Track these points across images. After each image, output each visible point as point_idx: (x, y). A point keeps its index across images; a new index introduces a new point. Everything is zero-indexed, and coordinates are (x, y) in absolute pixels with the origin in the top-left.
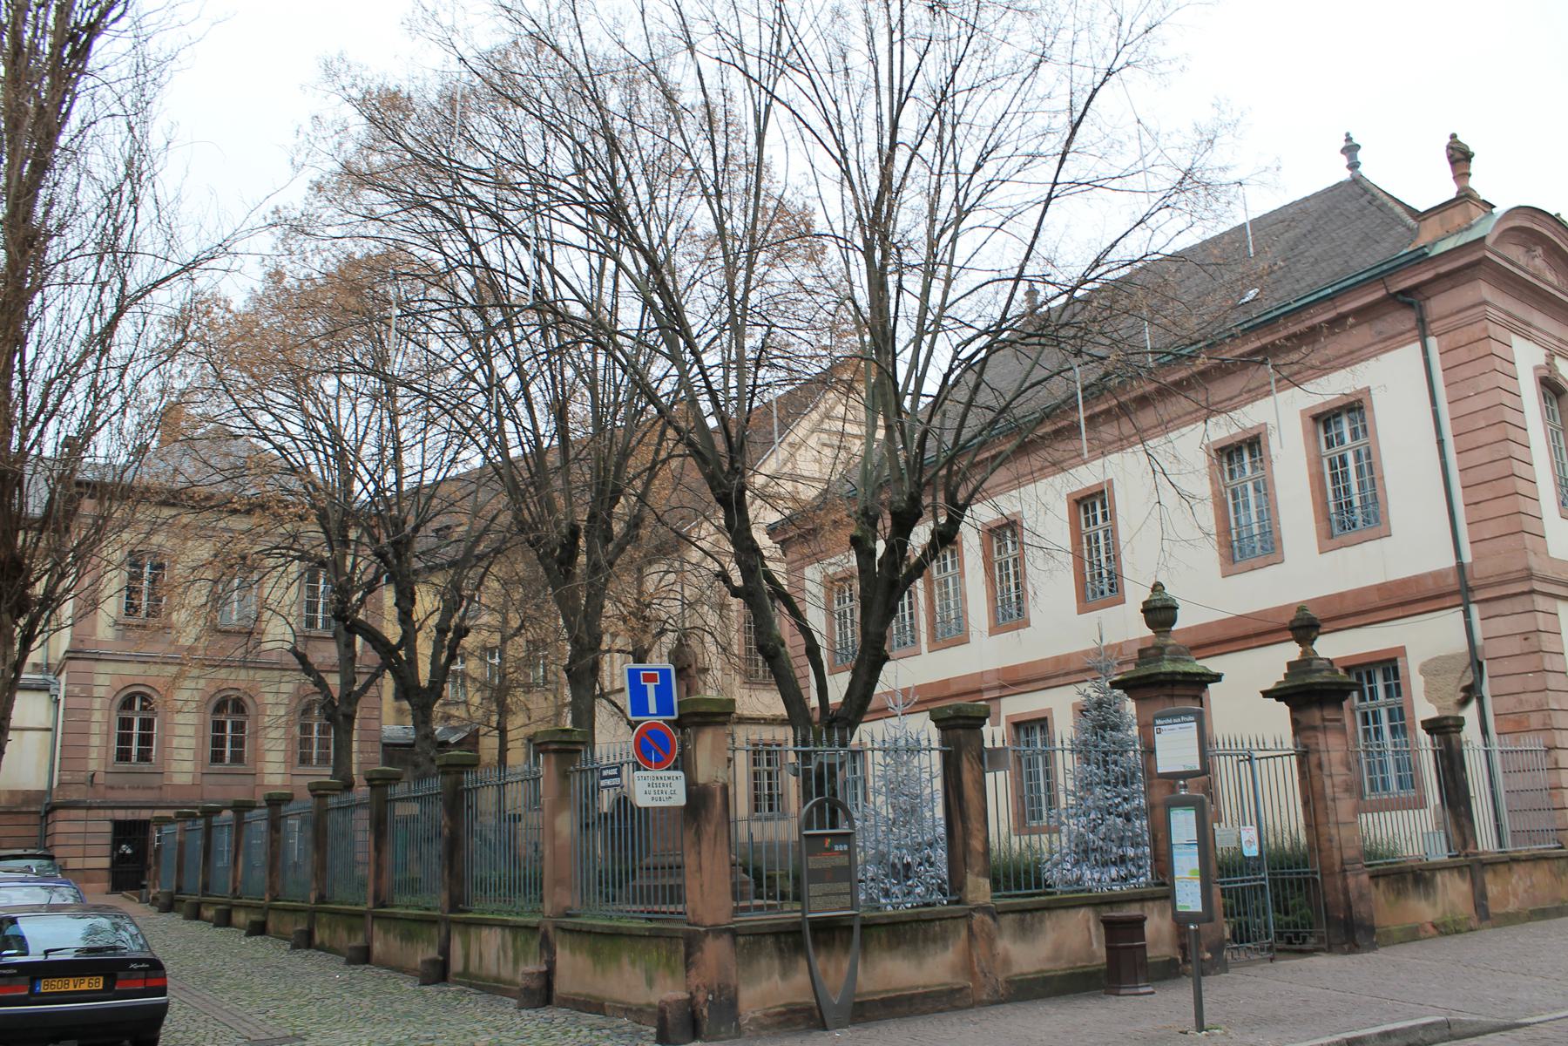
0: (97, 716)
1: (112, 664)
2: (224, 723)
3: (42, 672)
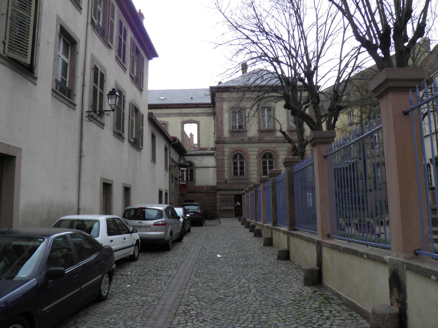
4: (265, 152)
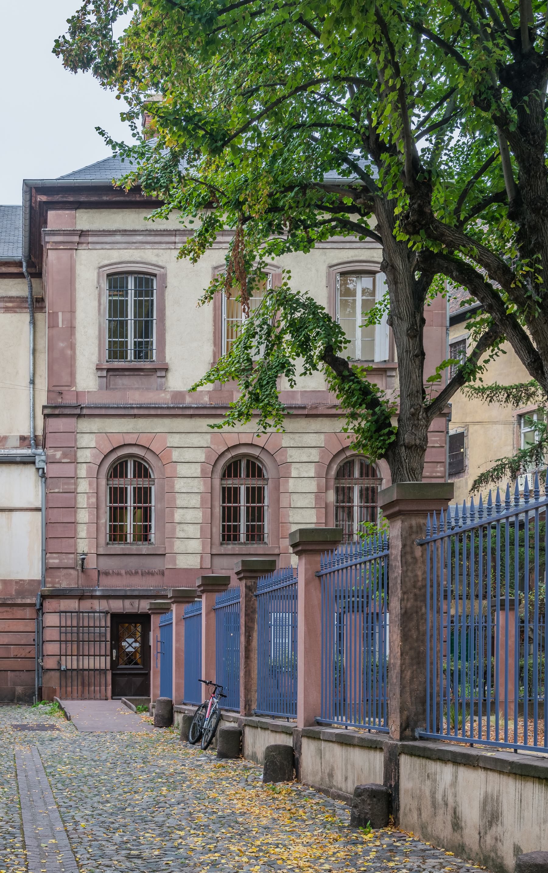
0: (83, 486)
1: (97, 420)
2: (236, 490)
3: (29, 446)
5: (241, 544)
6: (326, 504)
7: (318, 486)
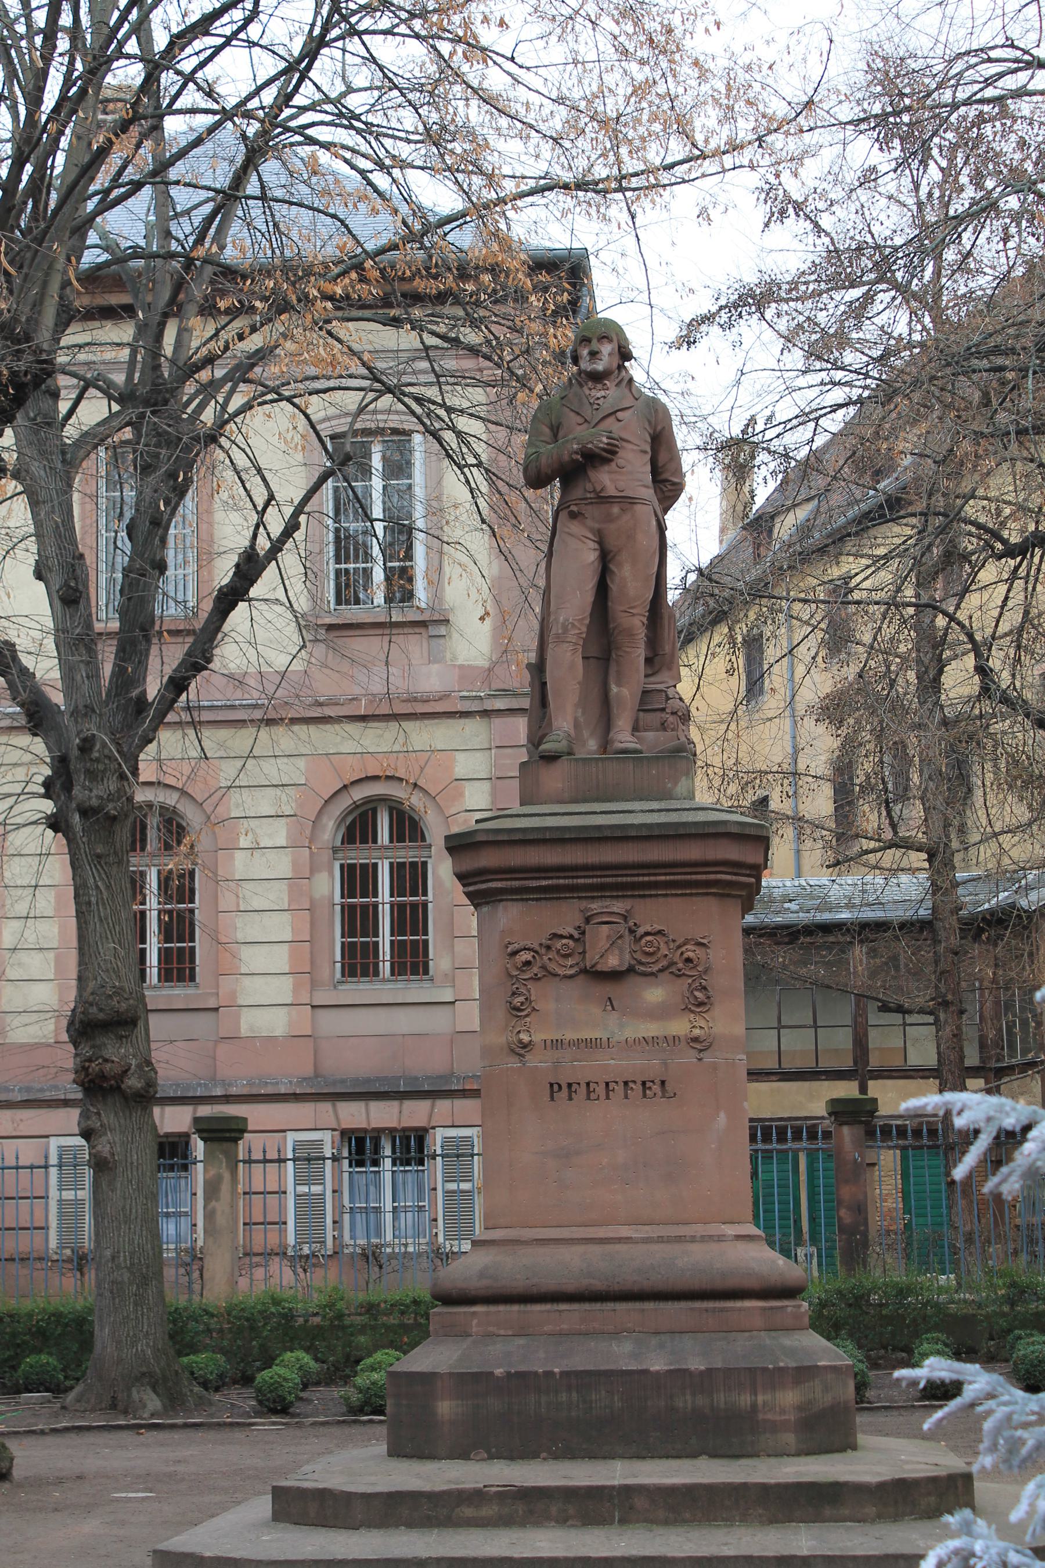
4: (359, 794)
5: (384, 980)
6: (312, 901)
7: (295, 864)
